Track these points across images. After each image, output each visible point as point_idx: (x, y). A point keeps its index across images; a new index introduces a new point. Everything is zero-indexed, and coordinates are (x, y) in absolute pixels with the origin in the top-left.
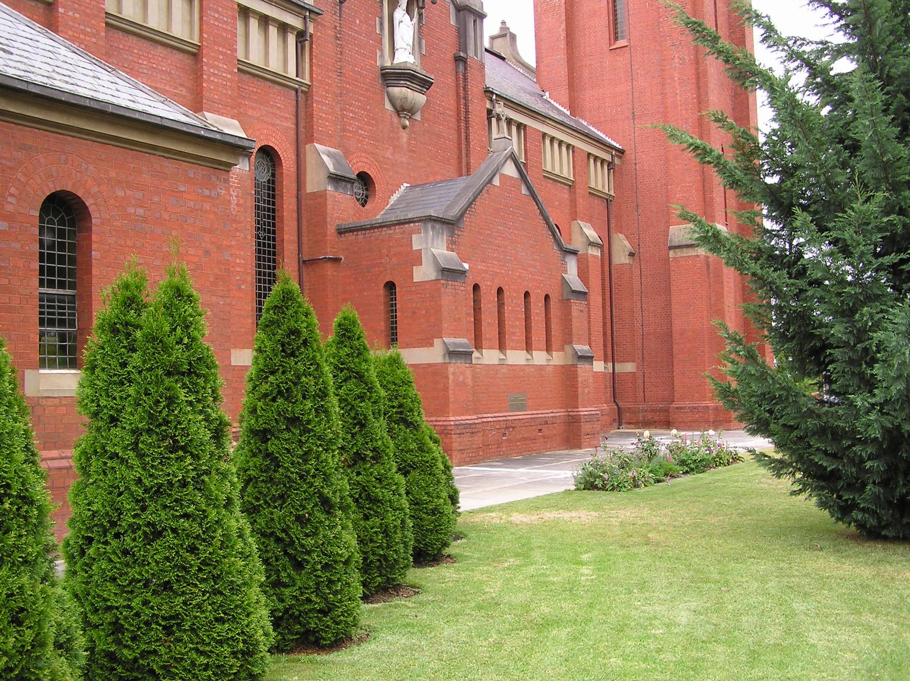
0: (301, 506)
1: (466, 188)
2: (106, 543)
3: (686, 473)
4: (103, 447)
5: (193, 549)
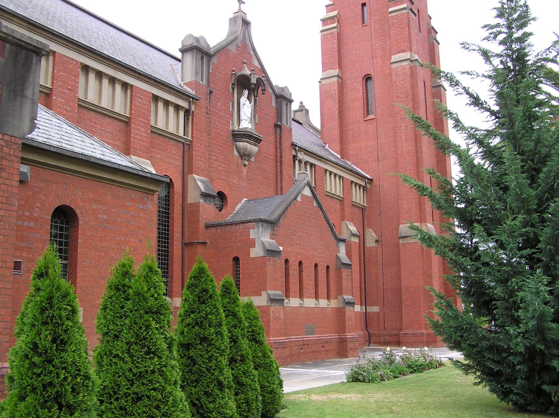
0: (207, 386)
1: (282, 202)
2: (111, 403)
3: (412, 372)
4: (110, 351)
5: (157, 407)
